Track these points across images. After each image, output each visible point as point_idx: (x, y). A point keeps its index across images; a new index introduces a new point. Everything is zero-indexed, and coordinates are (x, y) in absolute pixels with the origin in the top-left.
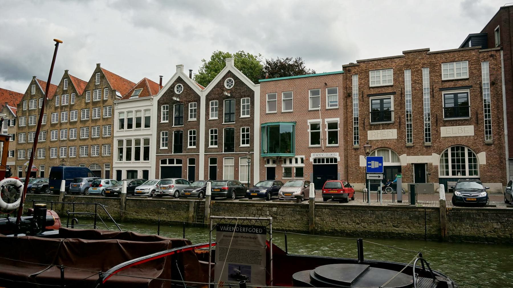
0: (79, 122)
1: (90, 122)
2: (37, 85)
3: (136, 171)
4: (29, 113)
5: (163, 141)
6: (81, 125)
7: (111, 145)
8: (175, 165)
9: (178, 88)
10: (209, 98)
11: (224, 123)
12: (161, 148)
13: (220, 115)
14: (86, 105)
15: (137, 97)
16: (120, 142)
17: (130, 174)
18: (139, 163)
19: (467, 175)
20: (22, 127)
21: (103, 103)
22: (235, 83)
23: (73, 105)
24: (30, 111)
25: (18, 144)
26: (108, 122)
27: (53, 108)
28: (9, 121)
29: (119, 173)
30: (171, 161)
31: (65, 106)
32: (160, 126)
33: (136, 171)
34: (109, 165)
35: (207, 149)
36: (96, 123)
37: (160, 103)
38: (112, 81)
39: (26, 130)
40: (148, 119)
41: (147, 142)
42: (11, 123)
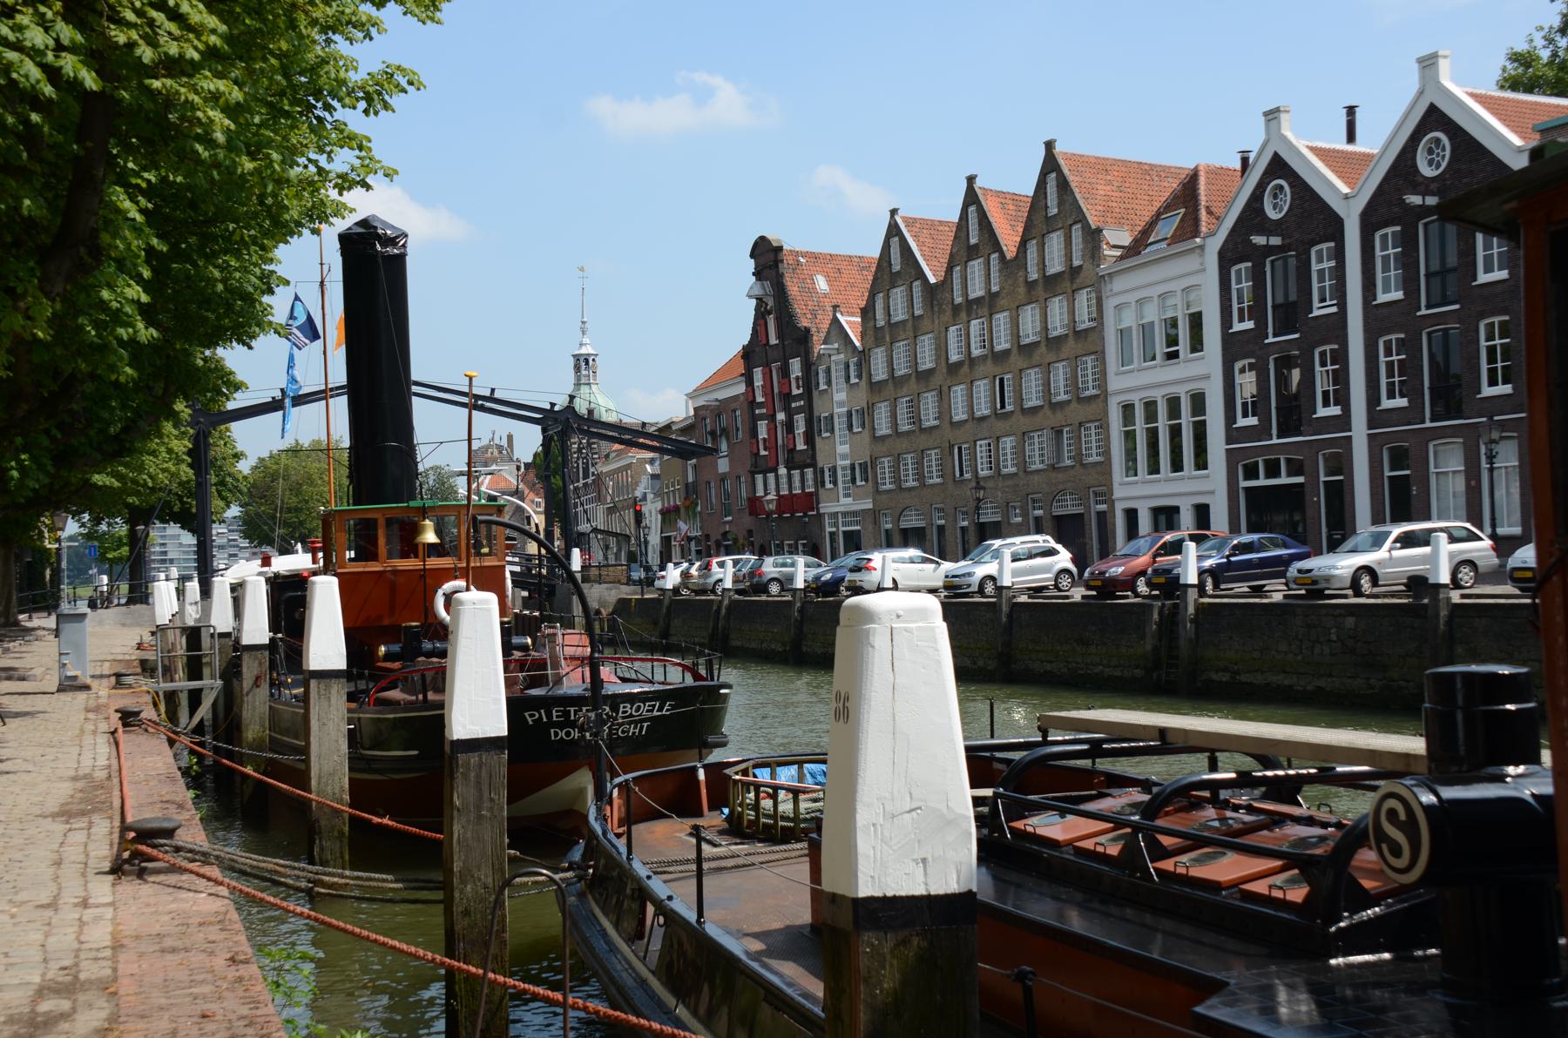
0: (1015, 351)
1: (1043, 349)
2: (903, 240)
3: (1176, 509)
4: (892, 337)
5: (1390, 374)
6: (1021, 364)
7: (1103, 426)
8: (1284, 480)
9: (1430, 151)
10: (1371, 221)
11: (1424, 312)
12: (1387, 403)
13: (1409, 283)
14: (1029, 291)
15: (1163, 245)
16: (1128, 409)
17: (1162, 519)
18: (1182, 478)
19: (1244, 484)
20: (1085, 330)
21: (1072, 280)
22: (1453, 151)
23: (997, 294)
24: (892, 326)
25: (876, 439)
26: (1087, 339)
27: (949, 313)
28: (847, 366)
29: (1132, 515)
30: (1273, 470)
31: (978, 300)
32: (1233, 347)
33: (1176, 509)
34: (1106, 496)
35: (1376, 418)
36: (1030, 356)
37: (1227, 259)
38: (1102, 190)
39: (889, 391)
40: (1196, 321)
41: (1198, 402)
42: (852, 374)
